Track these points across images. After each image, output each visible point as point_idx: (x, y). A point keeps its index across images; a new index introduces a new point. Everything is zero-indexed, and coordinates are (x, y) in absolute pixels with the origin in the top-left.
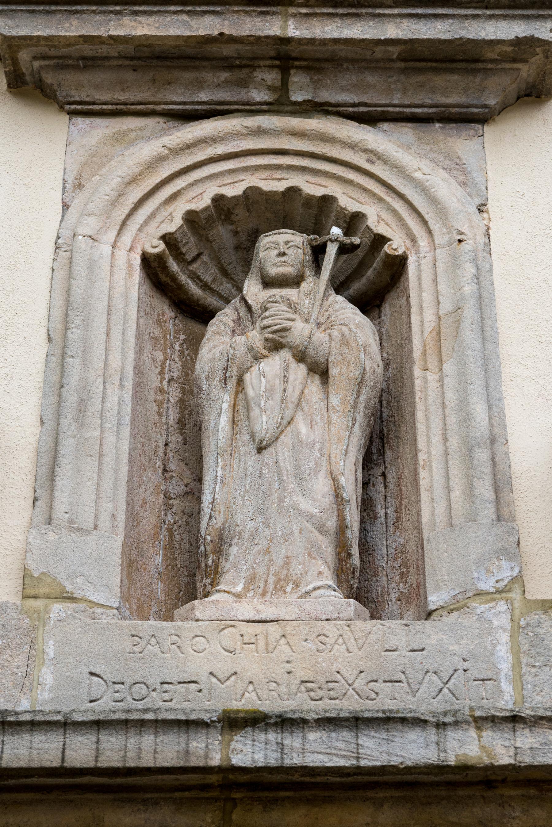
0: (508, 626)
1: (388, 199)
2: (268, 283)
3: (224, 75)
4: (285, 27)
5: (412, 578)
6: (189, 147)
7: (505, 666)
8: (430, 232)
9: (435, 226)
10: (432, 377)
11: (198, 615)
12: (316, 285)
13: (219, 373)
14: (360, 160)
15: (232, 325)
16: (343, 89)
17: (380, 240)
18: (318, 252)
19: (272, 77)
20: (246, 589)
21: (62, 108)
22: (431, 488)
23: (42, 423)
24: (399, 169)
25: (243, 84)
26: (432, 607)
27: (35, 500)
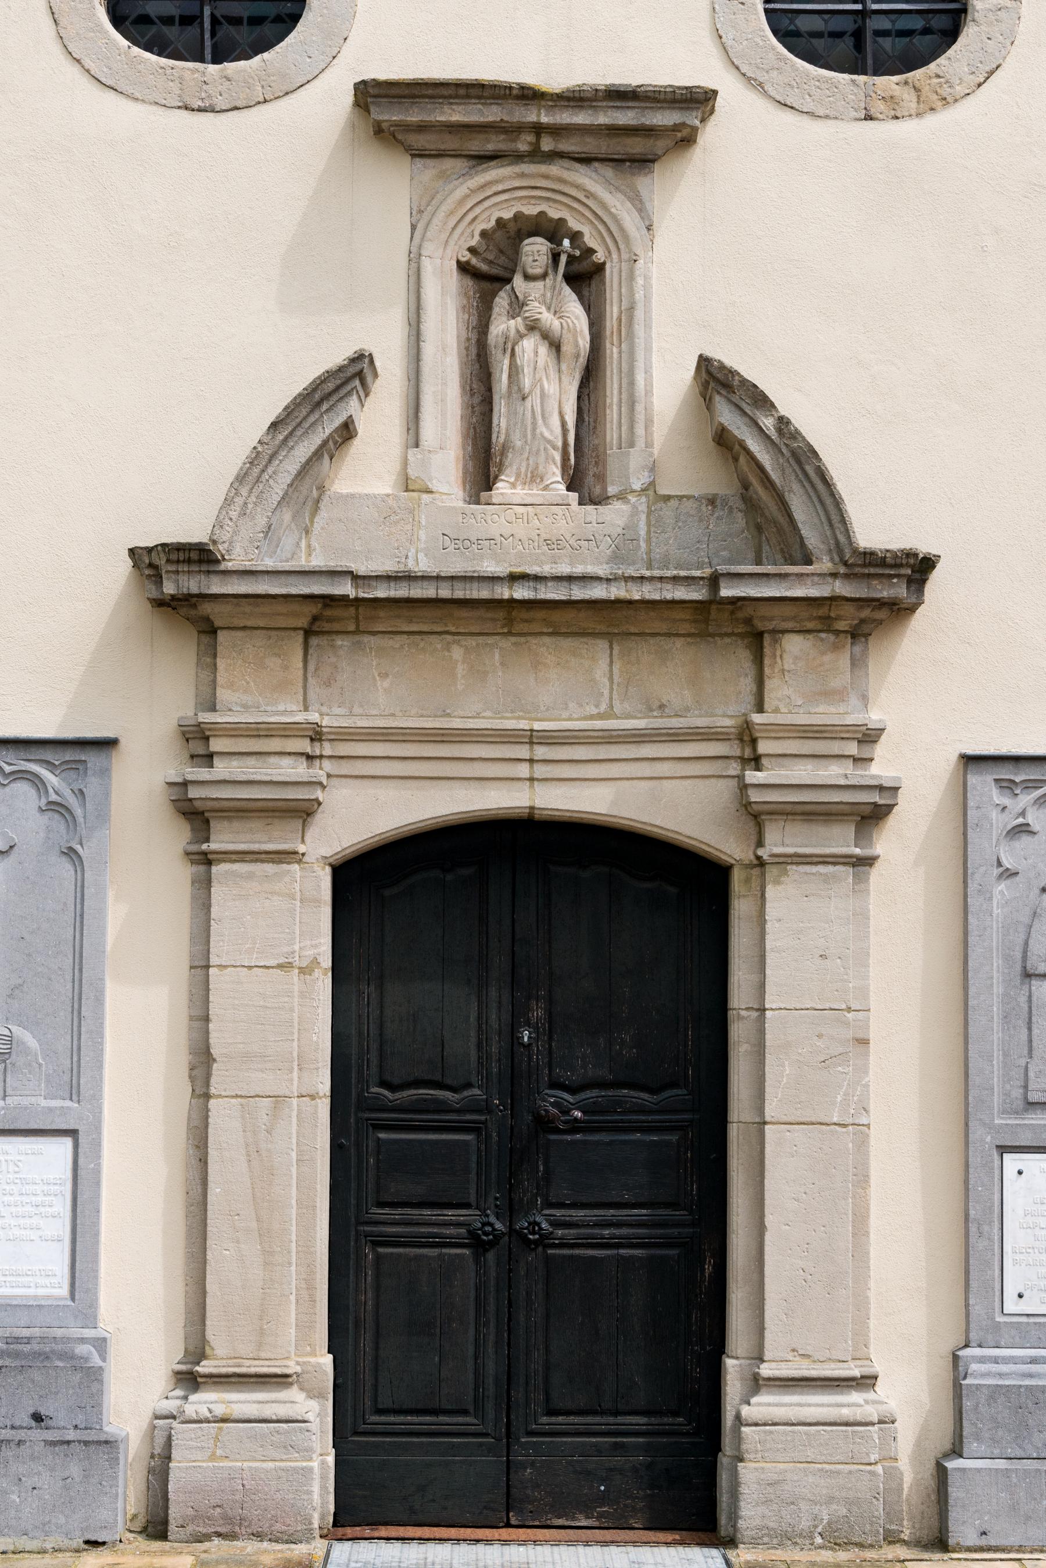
0: (646, 510)
1: (596, 223)
2: (527, 277)
3: (502, 137)
4: (539, 115)
5: (600, 468)
6: (482, 187)
7: (643, 533)
8: (619, 249)
9: (622, 246)
10: (615, 350)
11: (494, 501)
12: (555, 280)
13: (501, 345)
14: (581, 196)
15: (507, 307)
16: (572, 144)
17: (591, 251)
18: (555, 257)
19: (531, 138)
20: (516, 480)
21: (407, 150)
22: (612, 422)
23: (409, 380)
24: (604, 206)
25: (514, 141)
26: (609, 494)
27: (408, 429)
